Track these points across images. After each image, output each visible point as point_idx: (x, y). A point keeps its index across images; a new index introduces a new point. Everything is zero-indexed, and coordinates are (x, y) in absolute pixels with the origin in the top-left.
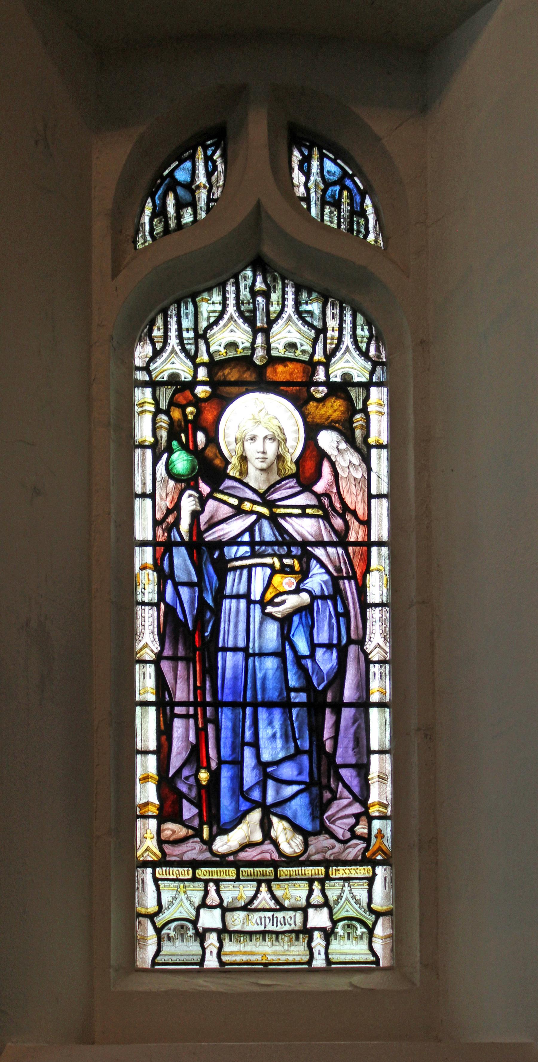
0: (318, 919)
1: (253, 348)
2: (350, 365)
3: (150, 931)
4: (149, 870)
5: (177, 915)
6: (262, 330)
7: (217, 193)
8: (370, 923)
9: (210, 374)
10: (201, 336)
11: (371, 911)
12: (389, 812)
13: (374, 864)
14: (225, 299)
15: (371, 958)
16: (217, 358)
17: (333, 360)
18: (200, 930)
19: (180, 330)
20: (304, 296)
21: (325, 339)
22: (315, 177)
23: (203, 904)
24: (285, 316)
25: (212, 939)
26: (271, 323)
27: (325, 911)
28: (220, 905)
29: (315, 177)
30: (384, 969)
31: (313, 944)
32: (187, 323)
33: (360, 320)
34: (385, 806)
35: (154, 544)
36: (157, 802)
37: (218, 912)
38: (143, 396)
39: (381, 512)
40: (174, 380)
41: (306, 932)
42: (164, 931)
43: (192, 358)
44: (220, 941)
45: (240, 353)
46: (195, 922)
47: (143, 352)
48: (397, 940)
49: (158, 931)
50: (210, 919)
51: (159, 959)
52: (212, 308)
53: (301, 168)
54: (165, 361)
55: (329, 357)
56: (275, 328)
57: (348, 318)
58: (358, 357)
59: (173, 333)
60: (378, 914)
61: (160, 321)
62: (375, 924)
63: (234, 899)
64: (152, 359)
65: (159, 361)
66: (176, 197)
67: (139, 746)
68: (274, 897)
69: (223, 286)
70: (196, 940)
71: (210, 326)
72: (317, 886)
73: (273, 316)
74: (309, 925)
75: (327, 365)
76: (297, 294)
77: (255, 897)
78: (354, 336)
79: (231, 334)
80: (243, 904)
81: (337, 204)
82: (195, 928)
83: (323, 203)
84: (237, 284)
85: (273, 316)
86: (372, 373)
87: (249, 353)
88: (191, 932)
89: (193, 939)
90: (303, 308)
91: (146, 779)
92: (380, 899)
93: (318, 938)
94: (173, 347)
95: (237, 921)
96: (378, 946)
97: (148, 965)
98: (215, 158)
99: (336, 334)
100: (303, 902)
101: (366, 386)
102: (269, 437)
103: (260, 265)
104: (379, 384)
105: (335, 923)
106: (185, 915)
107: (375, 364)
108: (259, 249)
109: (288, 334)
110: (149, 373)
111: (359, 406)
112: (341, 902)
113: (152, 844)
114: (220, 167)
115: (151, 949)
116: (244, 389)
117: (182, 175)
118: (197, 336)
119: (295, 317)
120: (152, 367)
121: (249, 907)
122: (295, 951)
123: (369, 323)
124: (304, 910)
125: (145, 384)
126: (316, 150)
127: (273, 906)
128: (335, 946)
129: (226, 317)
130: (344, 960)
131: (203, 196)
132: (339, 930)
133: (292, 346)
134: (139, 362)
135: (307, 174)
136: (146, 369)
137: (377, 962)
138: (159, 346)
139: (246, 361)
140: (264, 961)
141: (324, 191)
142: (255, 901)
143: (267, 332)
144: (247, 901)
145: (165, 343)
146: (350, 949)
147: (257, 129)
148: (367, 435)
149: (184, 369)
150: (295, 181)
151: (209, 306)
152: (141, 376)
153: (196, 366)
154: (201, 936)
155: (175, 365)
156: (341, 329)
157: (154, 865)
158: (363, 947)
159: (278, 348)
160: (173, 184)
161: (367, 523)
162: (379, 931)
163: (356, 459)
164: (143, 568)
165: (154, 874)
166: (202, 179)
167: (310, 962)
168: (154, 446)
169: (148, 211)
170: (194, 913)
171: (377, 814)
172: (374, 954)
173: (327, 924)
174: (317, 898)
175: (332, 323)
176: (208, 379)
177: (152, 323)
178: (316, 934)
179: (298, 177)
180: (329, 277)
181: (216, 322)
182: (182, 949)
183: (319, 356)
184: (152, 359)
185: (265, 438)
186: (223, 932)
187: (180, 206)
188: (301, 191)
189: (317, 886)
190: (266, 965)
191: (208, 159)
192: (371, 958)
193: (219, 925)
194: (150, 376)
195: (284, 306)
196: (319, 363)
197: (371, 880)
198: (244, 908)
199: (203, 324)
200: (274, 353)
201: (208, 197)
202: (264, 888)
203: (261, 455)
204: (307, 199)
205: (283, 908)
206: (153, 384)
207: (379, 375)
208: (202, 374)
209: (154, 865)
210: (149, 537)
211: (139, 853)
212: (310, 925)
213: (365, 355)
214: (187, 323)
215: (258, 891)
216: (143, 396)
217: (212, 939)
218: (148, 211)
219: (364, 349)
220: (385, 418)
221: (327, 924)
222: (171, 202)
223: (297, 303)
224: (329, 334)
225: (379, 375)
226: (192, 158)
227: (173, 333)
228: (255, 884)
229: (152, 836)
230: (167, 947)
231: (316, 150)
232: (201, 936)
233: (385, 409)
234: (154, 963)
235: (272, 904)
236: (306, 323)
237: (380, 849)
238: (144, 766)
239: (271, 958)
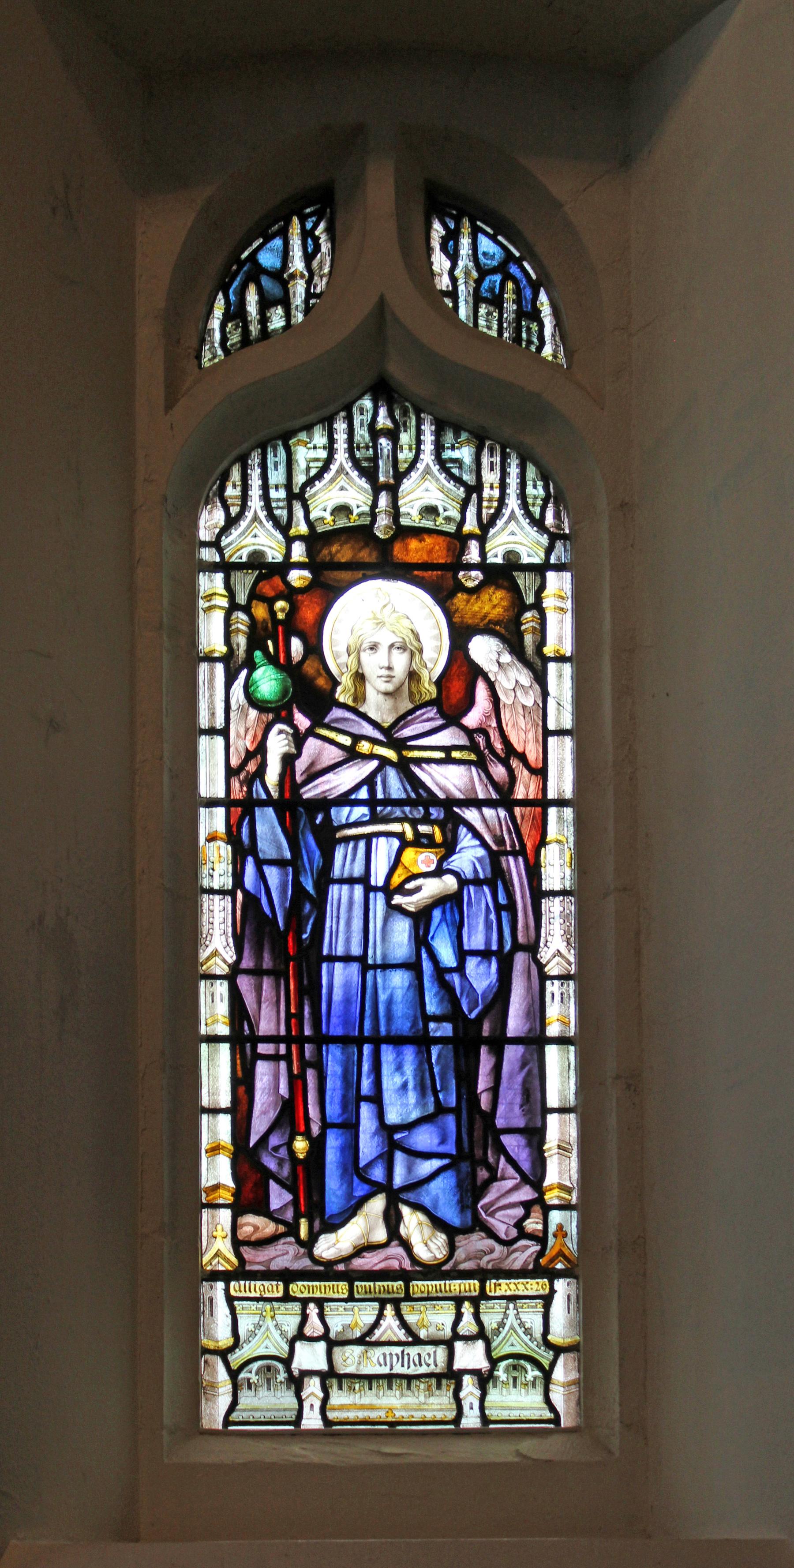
0: (470, 1356)
1: (373, 514)
2: (516, 539)
3: (222, 1374)
4: (220, 1285)
5: (261, 1352)
6: (387, 487)
7: (320, 285)
8: (546, 1363)
9: (309, 552)
10: (297, 496)
11: (548, 1345)
12: (574, 1199)
13: (553, 1275)
14: (332, 441)
15: (548, 1415)
16: (320, 529)
17: (492, 531)
18: (296, 1373)
19: (265, 487)
20: (449, 438)
21: (480, 500)
22: (465, 261)
23: (300, 1335)
24: (420, 466)
25: (313, 1386)
26: (399, 476)
27: (480, 1344)
28: (325, 1337)
29: (465, 261)
30: (567, 1430)
31: (462, 1395)
32: (277, 477)
33: (531, 472)
34: (569, 1190)
35: (227, 803)
36: (231, 1184)
37: (322, 1346)
38: (212, 584)
39: (562, 757)
40: (256, 561)
41: (451, 1376)
42: (242, 1375)
43: (284, 528)
44: (325, 1389)
45: (354, 520)
46: (287, 1362)
47: (211, 519)
48: (586, 1388)
49: (233, 1374)
50: (311, 1357)
51: (234, 1417)
52: (312, 454)
53: (444, 248)
54: (243, 533)
55: (485, 527)
56: (406, 485)
57: (514, 470)
58: (528, 528)
59: (255, 492)
60: (558, 1350)
61: (236, 474)
62: (553, 1364)
63: (346, 1327)
64: (225, 530)
65: (235, 533)
66: (260, 291)
67: (205, 1102)
68: (404, 1324)
69: (328, 422)
70: (289, 1388)
71: (310, 482)
72: (467, 1309)
73: (403, 467)
74: (456, 1366)
75: (482, 540)
76: (438, 434)
77: (376, 1325)
78: (523, 496)
79: (341, 494)
80: (358, 1334)
81: (497, 302)
82: (289, 1370)
83: (477, 299)
84: (350, 420)
85: (403, 467)
86: (549, 551)
87: (367, 521)
88: (282, 1376)
89: (284, 1387)
90: (448, 454)
91: (215, 1150)
92: (561, 1328)
93: (469, 1384)
94: (255, 512)
95: (350, 1359)
96: (558, 1396)
97: (219, 1425)
98: (317, 233)
99: (496, 493)
100: (448, 1332)
101: (540, 570)
102: (397, 645)
103: (384, 391)
104: (559, 568)
105: (494, 1363)
106: (273, 1351)
107: (554, 538)
108: (382, 367)
109: (425, 493)
110: (220, 550)
111: (530, 600)
112: (504, 1332)
113: (224, 1246)
114: (325, 247)
115: (224, 1401)
116: (360, 574)
117: (268, 259)
118: (291, 497)
119: (435, 469)
120: (224, 542)
121: (368, 1339)
122: (436, 1405)
123: (545, 477)
124: (449, 1344)
125: (213, 568)
126: (466, 222)
127: (403, 1338)
128: (494, 1396)
129: (334, 468)
130: (508, 1418)
131: (299, 289)
132: (501, 1373)
133: (430, 511)
134: (205, 535)
135: (454, 258)
136: (215, 544)
137: (556, 1420)
138: (234, 510)
139: (363, 533)
140: (390, 1419)
141: (479, 282)
142: (376, 1331)
143: (393, 490)
144: (365, 1330)
145: (244, 506)
146: (517, 1401)
147: (380, 191)
148: (542, 643)
149: (271, 546)
150: (436, 268)
151: (308, 452)
152: (208, 555)
153: (289, 541)
154: (296, 1382)
155: (259, 539)
156: (503, 486)
157: (227, 1277)
158: (535, 1398)
159: (411, 514)
160: (256, 272)
161: (541, 772)
162: (559, 1374)
163: (525, 677)
164: (212, 838)
165: (227, 1290)
166: (298, 264)
167: (457, 1420)
168: (227, 659)
169: (218, 312)
170: (286, 1348)
171: (556, 1202)
172: (552, 1408)
173: (483, 1364)
174: (468, 1325)
175: (490, 477)
176: (307, 560)
177: (225, 477)
178: (467, 1379)
179: (440, 262)
180: (485, 409)
181: (319, 476)
182: (268, 1401)
183: (471, 526)
184: (225, 530)
185: (392, 646)
186: (330, 1376)
187: (265, 304)
188: (444, 283)
189: (467, 1309)
190: (392, 1424)
191: (307, 234)
192: (548, 1415)
193: (323, 1366)
194: (222, 555)
195: (418, 451)
196: (471, 536)
197: (547, 1300)
198: (360, 1341)
199: (300, 479)
200: (404, 521)
201: (307, 290)
202: (389, 1311)
203: (385, 672)
204: (453, 294)
205: (417, 1341)
206: (226, 567)
207: (560, 553)
208: (298, 552)
209: (227, 1277)
210: (220, 792)
211: (205, 1259)
212: (457, 1365)
213: (539, 523)
214: (277, 477)
215: (380, 1316)
216: (212, 584)
217: (313, 1386)
218: (218, 312)
219: (537, 516)
220: (568, 618)
221: (483, 1364)
222: (252, 298)
223: (439, 448)
224: (486, 493)
225: (560, 553)
226: (284, 234)
227: (255, 492)
228: (376, 1305)
229: (224, 1234)
230: (246, 1399)
231: (466, 222)
232: (296, 1382)
233: (569, 605)
234: (227, 1422)
235: (401, 1335)
236: (451, 476)
237: (561, 1254)
238: (213, 1131)
239: (399, 1415)
